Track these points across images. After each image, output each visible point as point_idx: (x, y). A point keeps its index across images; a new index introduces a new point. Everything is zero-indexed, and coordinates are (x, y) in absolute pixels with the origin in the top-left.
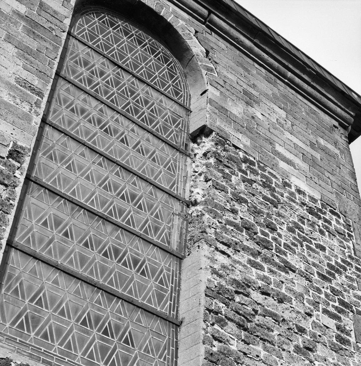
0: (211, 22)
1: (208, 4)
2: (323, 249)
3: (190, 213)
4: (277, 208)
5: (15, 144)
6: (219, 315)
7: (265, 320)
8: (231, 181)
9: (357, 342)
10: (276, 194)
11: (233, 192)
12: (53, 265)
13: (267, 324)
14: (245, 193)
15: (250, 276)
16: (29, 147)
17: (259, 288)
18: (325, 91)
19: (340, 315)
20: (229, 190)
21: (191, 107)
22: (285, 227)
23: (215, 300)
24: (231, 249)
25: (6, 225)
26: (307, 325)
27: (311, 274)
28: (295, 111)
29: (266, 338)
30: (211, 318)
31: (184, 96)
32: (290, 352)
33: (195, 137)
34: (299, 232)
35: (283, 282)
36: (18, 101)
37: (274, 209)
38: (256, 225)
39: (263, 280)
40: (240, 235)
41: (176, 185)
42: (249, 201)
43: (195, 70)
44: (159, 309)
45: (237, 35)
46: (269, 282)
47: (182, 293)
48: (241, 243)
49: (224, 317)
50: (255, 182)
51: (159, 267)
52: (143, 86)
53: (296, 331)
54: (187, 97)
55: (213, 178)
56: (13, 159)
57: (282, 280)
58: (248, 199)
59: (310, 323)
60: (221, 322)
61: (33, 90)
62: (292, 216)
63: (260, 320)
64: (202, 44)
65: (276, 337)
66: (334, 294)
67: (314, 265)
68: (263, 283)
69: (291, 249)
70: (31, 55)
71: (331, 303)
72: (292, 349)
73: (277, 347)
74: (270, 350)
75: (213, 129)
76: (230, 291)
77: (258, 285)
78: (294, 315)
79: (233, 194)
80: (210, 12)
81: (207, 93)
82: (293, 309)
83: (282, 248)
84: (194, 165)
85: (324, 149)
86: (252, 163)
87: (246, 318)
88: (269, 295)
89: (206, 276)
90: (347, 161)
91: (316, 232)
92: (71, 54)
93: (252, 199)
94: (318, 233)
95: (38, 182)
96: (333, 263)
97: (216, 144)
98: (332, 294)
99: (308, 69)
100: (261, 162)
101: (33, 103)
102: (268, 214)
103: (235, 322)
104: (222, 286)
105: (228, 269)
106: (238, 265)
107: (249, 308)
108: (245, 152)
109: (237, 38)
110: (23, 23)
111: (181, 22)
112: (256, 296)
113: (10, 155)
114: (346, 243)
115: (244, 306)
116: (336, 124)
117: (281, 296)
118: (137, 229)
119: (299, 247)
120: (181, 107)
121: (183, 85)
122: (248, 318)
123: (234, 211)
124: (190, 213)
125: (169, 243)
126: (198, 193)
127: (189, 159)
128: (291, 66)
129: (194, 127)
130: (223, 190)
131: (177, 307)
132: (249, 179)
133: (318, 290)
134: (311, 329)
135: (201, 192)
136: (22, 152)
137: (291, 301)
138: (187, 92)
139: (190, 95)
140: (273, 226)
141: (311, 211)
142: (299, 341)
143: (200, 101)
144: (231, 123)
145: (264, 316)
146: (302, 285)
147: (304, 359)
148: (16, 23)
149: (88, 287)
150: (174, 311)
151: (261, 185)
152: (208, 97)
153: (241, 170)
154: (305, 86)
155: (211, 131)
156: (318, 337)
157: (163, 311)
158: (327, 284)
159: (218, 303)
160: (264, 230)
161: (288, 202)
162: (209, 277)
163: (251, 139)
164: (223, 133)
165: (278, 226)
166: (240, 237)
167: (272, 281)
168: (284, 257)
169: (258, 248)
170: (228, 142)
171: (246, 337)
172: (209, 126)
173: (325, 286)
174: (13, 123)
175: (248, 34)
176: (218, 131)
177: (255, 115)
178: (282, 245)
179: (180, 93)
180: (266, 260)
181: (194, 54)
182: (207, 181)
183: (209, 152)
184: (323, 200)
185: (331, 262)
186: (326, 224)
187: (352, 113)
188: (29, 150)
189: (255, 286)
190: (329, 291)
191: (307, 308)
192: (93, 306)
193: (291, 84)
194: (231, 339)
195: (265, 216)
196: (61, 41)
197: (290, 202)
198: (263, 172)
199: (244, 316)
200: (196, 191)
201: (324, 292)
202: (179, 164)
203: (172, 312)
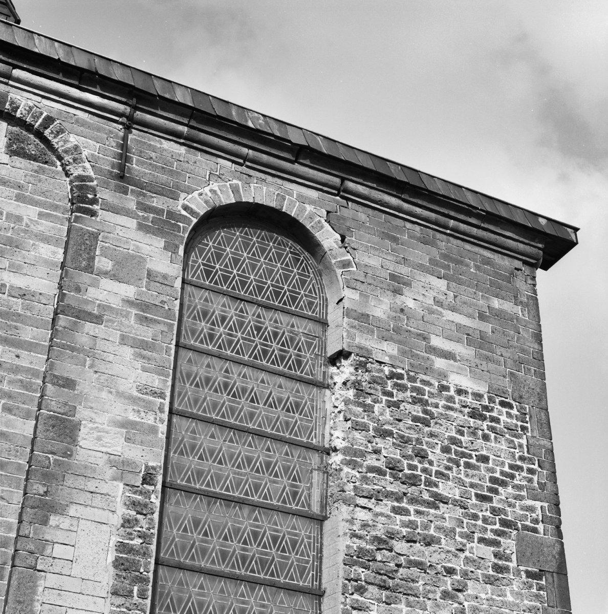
0: (347, 191)
1: (340, 171)
2: (485, 459)
3: (330, 463)
4: (429, 427)
5: (147, 467)
6: (359, 582)
7: (410, 572)
8: (373, 412)
9: (518, 566)
10: (429, 408)
11: (376, 427)
12: (198, 570)
13: (411, 577)
14: (391, 422)
15: (393, 527)
16: (159, 464)
17: (404, 536)
18: (501, 228)
19: (499, 538)
20: (372, 425)
21: (328, 318)
22: (438, 450)
23: (354, 568)
24: (373, 500)
25: (150, 557)
26: (458, 564)
27: (468, 499)
28: (459, 272)
29: (409, 592)
30: (351, 586)
31: (320, 304)
32: (436, 600)
33: (334, 360)
34: (456, 448)
35: (431, 521)
36: (143, 414)
37: (427, 429)
38: (402, 459)
39: (407, 527)
40: (382, 481)
41: (314, 431)
42: (395, 431)
43: (329, 268)
44: (301, 584)
45: (380, 197)
46: (414, 527)
47: (324, 560)
48: (384, 489)
49: (363, 583)
50: (403, 401)
51: (299, 537)
52: (270, 314)
53: (445, 574)
54: (323, 305)
55: (353, 418)
56: (147, 484)
57: (430, 519)
58: (393, 429)
59: (462, 559)
60: (361, 590)
61: (154, 394)
62: (449, 430)
63: (404, 574)
64: (335, 229)
65: (421, 588)
66: (495, 515)
67: (472, 485)
68: (409, 530)
69: (443, 475)
70: (148, 350)
71: (489, 527)
72: (439, 595)
73: (421, 599)
74: (413, 604)
75: (351, 351)
76: (371, 551)
77: (402, 535)
78: (443, 556)
79: (375, 430)
80: (343, 180)
81: (343, 301)
82: (442, 550)
83: (433, 478)
84: (333, 397)
85: (499, 315)
86: (400, 377)
87: (388, 576)
88: (415, 542)
89: (344, 543)
90: (531, 317)
91: (478, 440)
92: (188, 309)
93: (398, 427)
94: (481, 441)
95: (173, 487)
96: (497, 475)
97: (356, 369)
98: (492, 516)
99: (474, 211)
100: (411, 371)
101: (157, 411)
102: (417, 439)
103: (376, 585)
104: (362, 548)
105: (369, 526)
106: (380, 517)
107: (391, 565)
108: (393, 366)
109: (380, 201)
110: (134, 311)
111: (309, 208)
112: (400, 546)
113: (145, 481)
114: (518, 440)
115: (385, 563)
116: (518, 264)
117: (428, 540)
118: (275, 502)
119: (455, 469)
120: (316, 323)
121: (318, 288)
122: (391, 575)
123: (377, 452)
124: (330, 463)
125: (309, 506)
126: (338, 438)
127: (328, 392)
128: (452, 213)
129: (331, 350)
130: (363, 428)
131: (320, 576)
132: (395, 402)
133: (475, 517)
134: (462, 566)
135: (341, 435)
136: (154, 472)
137: (440, 541)
138: (323, 296)
139: (327, 300)
140: (422, 453)
141: (474, 414)
142: (448, 583)
143: (336, 312)
144: (373, 332)
145: (409, 568)
146: (454, 518)
147: (451, 603)
148: (127, 316)
149: (231, 582)
150: (316, 582)
151: (410, 403)
152: (344, 308)
153: (386, 393)
154: (474, 231)
155: (350, 354)
156: (470, 574)
157: (306, 584)
158: (487, 505)
159: (357, 569)
160: (412, 463)
161: (444, 412)
162: (348, 543)
163: (399, 342)
164: (364, 351)
165: (429, 451)
166: (383, 483)
167: (419, 524)
168: (435, 489)
169: (403, 488)
170: (370, 360)
171: (387, 597)
172: (346, 349)
173: (484, 509)
174: (142, 443)
175: (393, 191)
176: (357, 351)
177: (405, 305)
178: (433, 475)
179: (314, 302)
180: (413, 501)
181: (327, 249)
182: (346, 420)
183: (348, 381)
184: (491, 392)
185: (494, 475)
186: (493, 424)
187: (540, 246)
188: (160, 467)
189: (399, 536)
190: (488, 514)
191: (459, 543)
192: (238, 601)
193: (457, 234)
194: (371, 605)
195: (414, 443)
196: (175, 315)
197: (447, 412)
198: (414, 383)
199: (385, 575)
200: (336, 434)
201: (481, 517)
202: (317, 403)
203: (315, 583)
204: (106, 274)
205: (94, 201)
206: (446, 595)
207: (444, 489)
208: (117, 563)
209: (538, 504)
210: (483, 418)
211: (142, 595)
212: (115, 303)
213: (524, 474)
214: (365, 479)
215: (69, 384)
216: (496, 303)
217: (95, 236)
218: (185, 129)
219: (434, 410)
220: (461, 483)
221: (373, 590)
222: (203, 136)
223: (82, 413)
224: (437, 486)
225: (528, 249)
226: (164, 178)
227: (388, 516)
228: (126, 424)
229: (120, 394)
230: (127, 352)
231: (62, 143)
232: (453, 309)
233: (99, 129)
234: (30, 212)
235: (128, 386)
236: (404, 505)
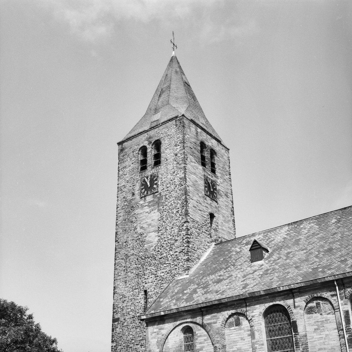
154: (155, 224)
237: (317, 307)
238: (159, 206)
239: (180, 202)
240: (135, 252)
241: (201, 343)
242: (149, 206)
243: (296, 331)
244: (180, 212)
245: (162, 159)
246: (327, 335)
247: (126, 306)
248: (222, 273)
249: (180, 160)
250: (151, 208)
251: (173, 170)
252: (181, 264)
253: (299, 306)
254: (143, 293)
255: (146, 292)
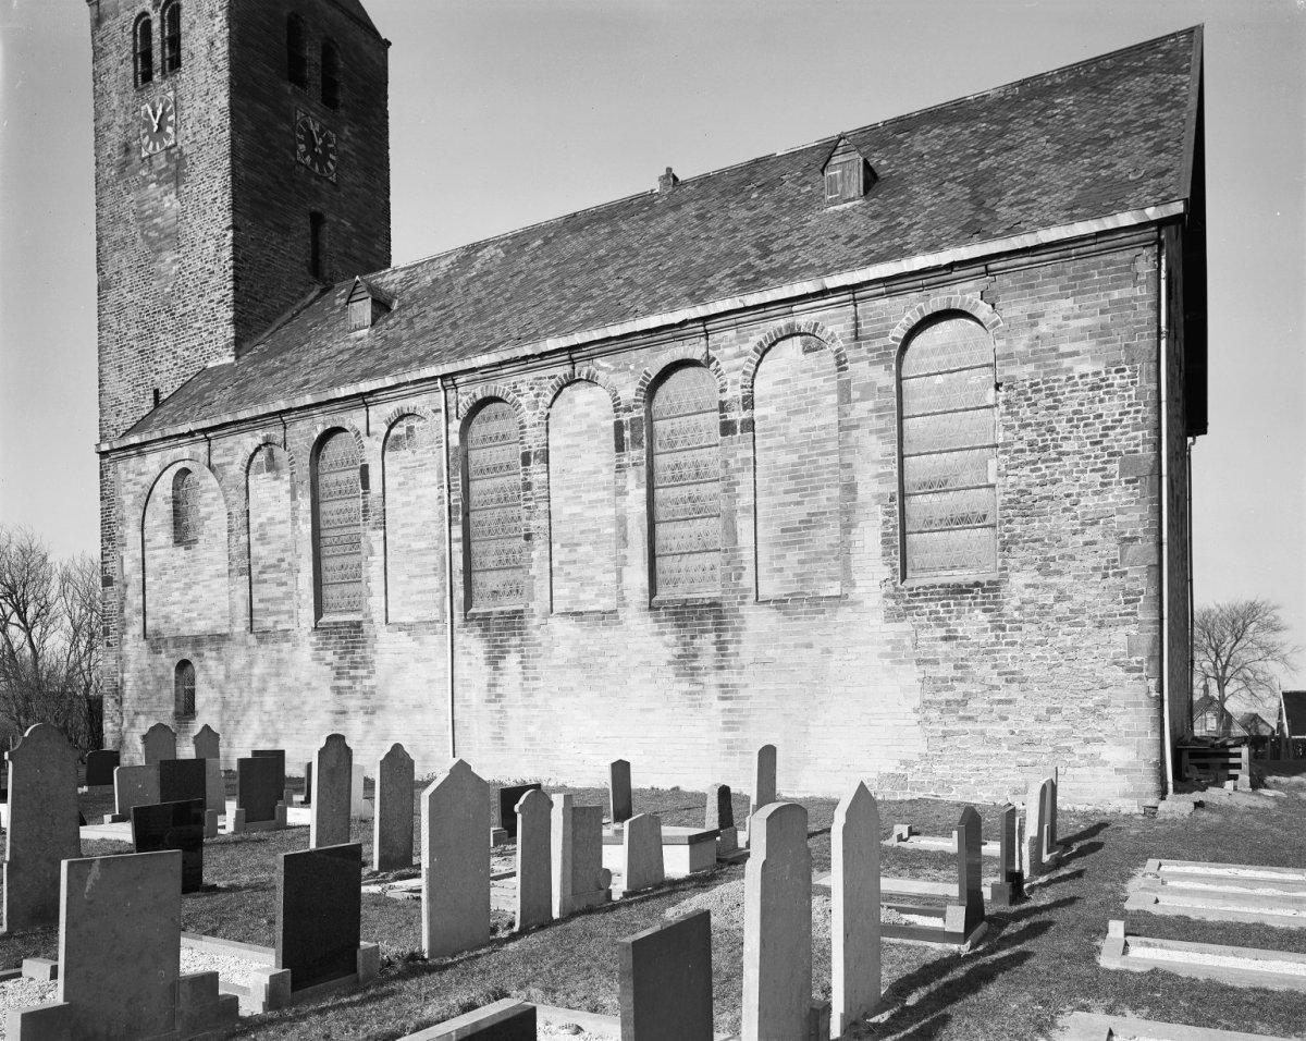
22: (1064, 423)
60: (1010, 522)
112: (1036, 490)
113: (891, 501)
154: (1093, 248)
187: (1153, 229)
204: (857, 400)
205: (846, 361)
206: (1065, 510)
207: (1066, 447)
208: (883, 542)
209: (1140, 433)
210: (1099, 388)
211: (896, 553)
212: (865, 415)
213: (1131, 415)
214: (1012, 459)
215: (849, 466)
216: (1116, 295)
217: (849, 381)
218: (883, 289)
219: (1062, 398)
220: (1080, 438)
221: (1019, 519)
222: (894, 288)
223: (858, 478)
224: (1061, 447)
225: (1143, 237)
226: (878, 325)
227: (1028, 476)
228: (879, 475)
229: (873, 462)
230: (874, 438)
231: (865, 629)
232: (1078, 317)
233: (841, 315)
234: (819, 382)
235: (877, 456)
236: (1038, 466)
237: (408, 436)
238: (177, 185)
239: (219, 175)
240: (137, 297)
241: (206, 505)
242: (159, 183)
243: (365, 485)
244: (219, 200)
245: (184, 53)
246: (418, 497)
247: (123, 424)
248: (288, 356)
249: (220, 57)
250: (162, 189)
251: (205, 87)
252: (220, 329)
253: (375, 433)
254: (152, 396)
255: (156, 392)
